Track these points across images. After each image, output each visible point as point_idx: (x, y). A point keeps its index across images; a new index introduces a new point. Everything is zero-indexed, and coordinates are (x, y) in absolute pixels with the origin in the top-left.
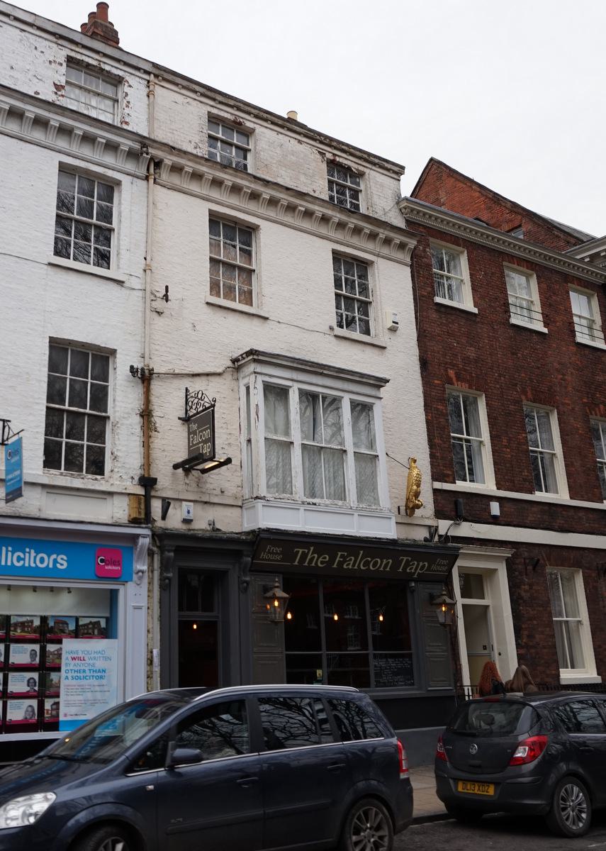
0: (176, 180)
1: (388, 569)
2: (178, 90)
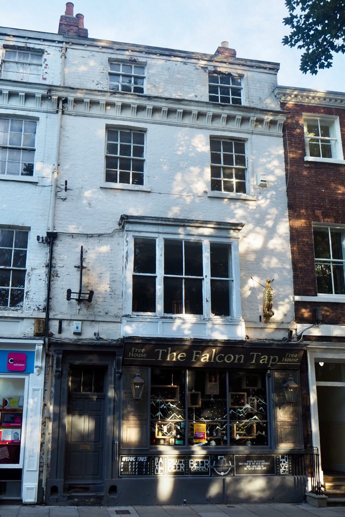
0: (81, 109)
1: (242, 362)
2: (158, 57)
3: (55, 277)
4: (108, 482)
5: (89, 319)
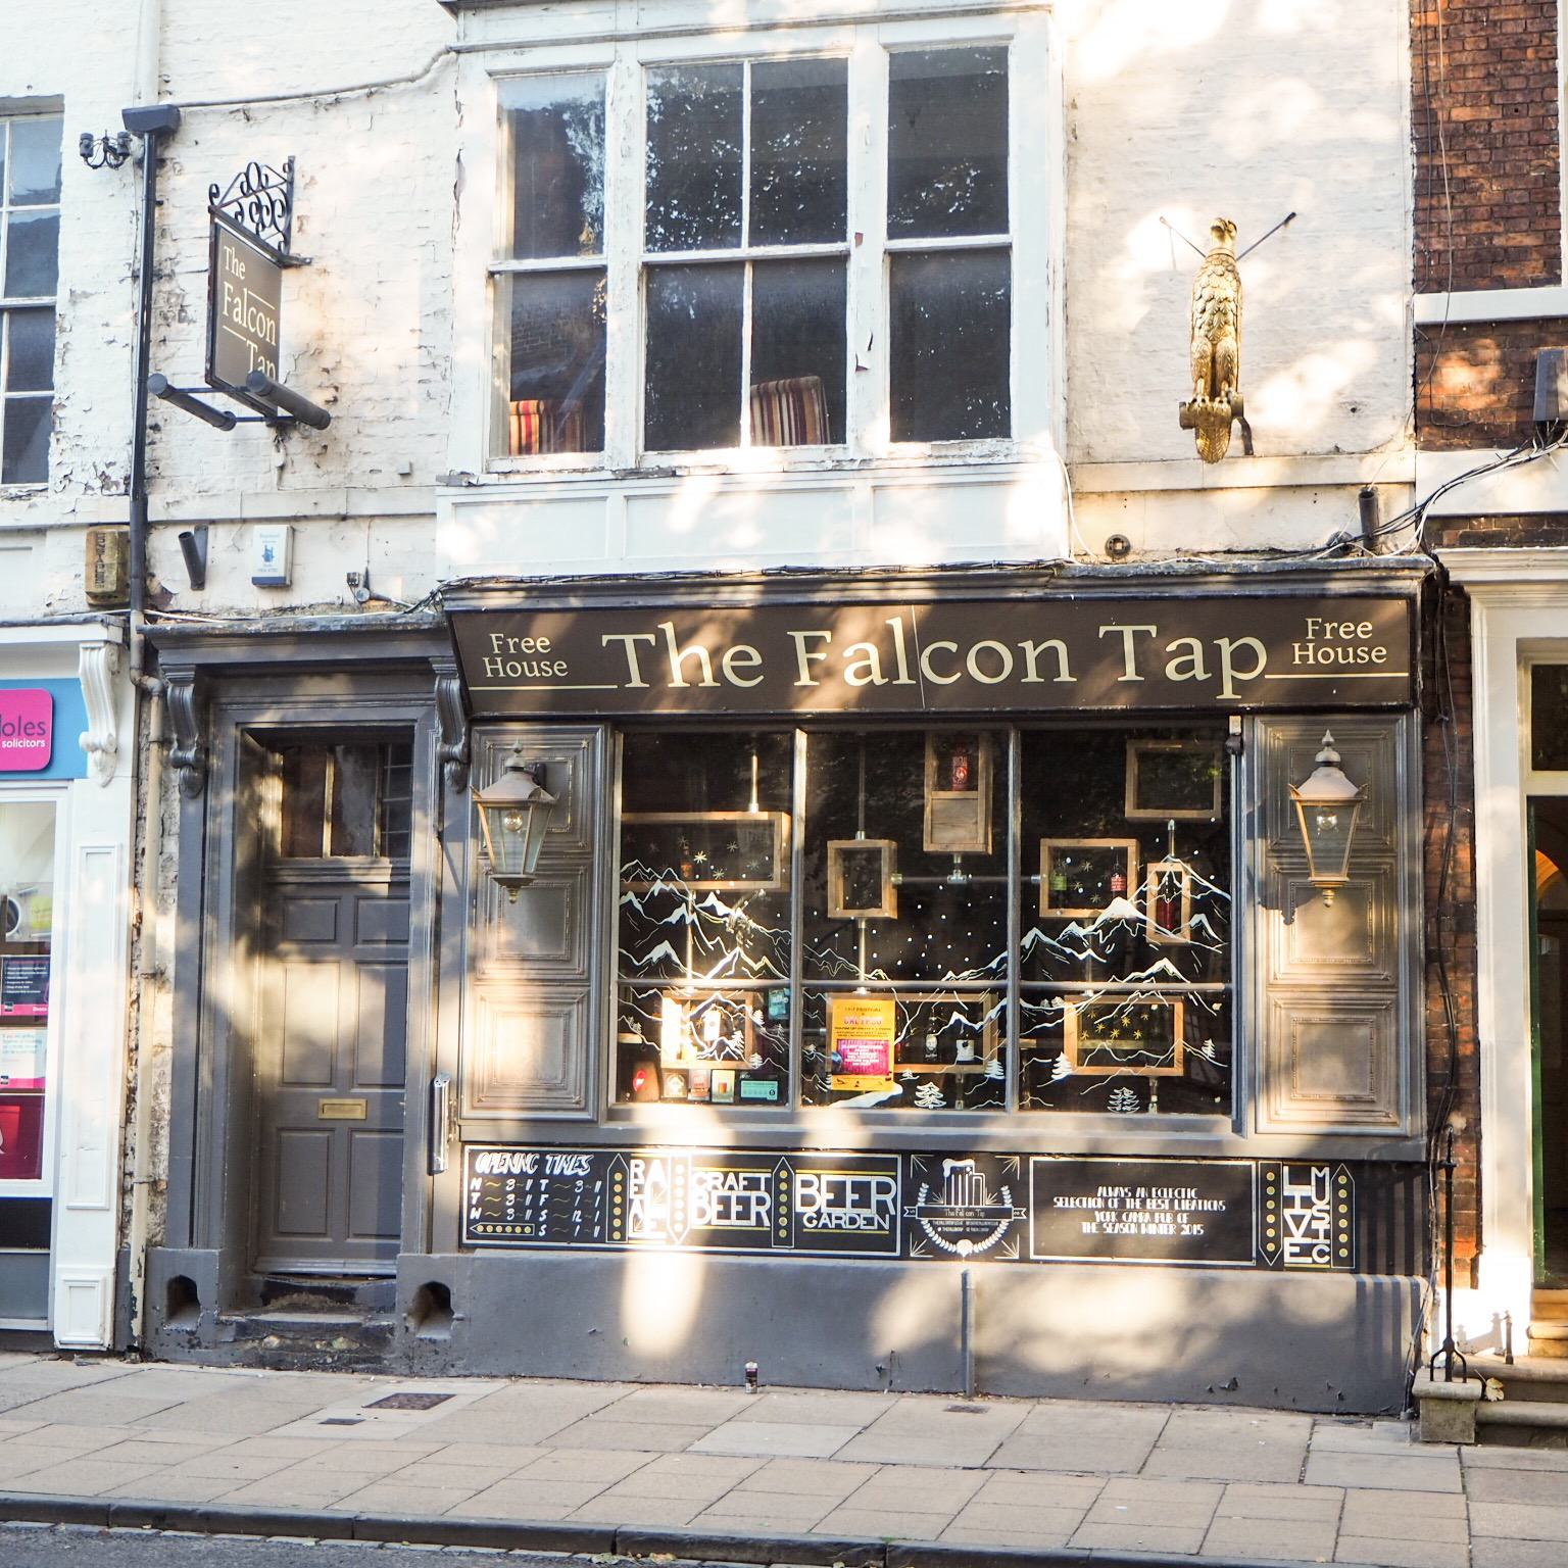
3: (175, 325)
4: (412, 1267)
5: (323, 511)
